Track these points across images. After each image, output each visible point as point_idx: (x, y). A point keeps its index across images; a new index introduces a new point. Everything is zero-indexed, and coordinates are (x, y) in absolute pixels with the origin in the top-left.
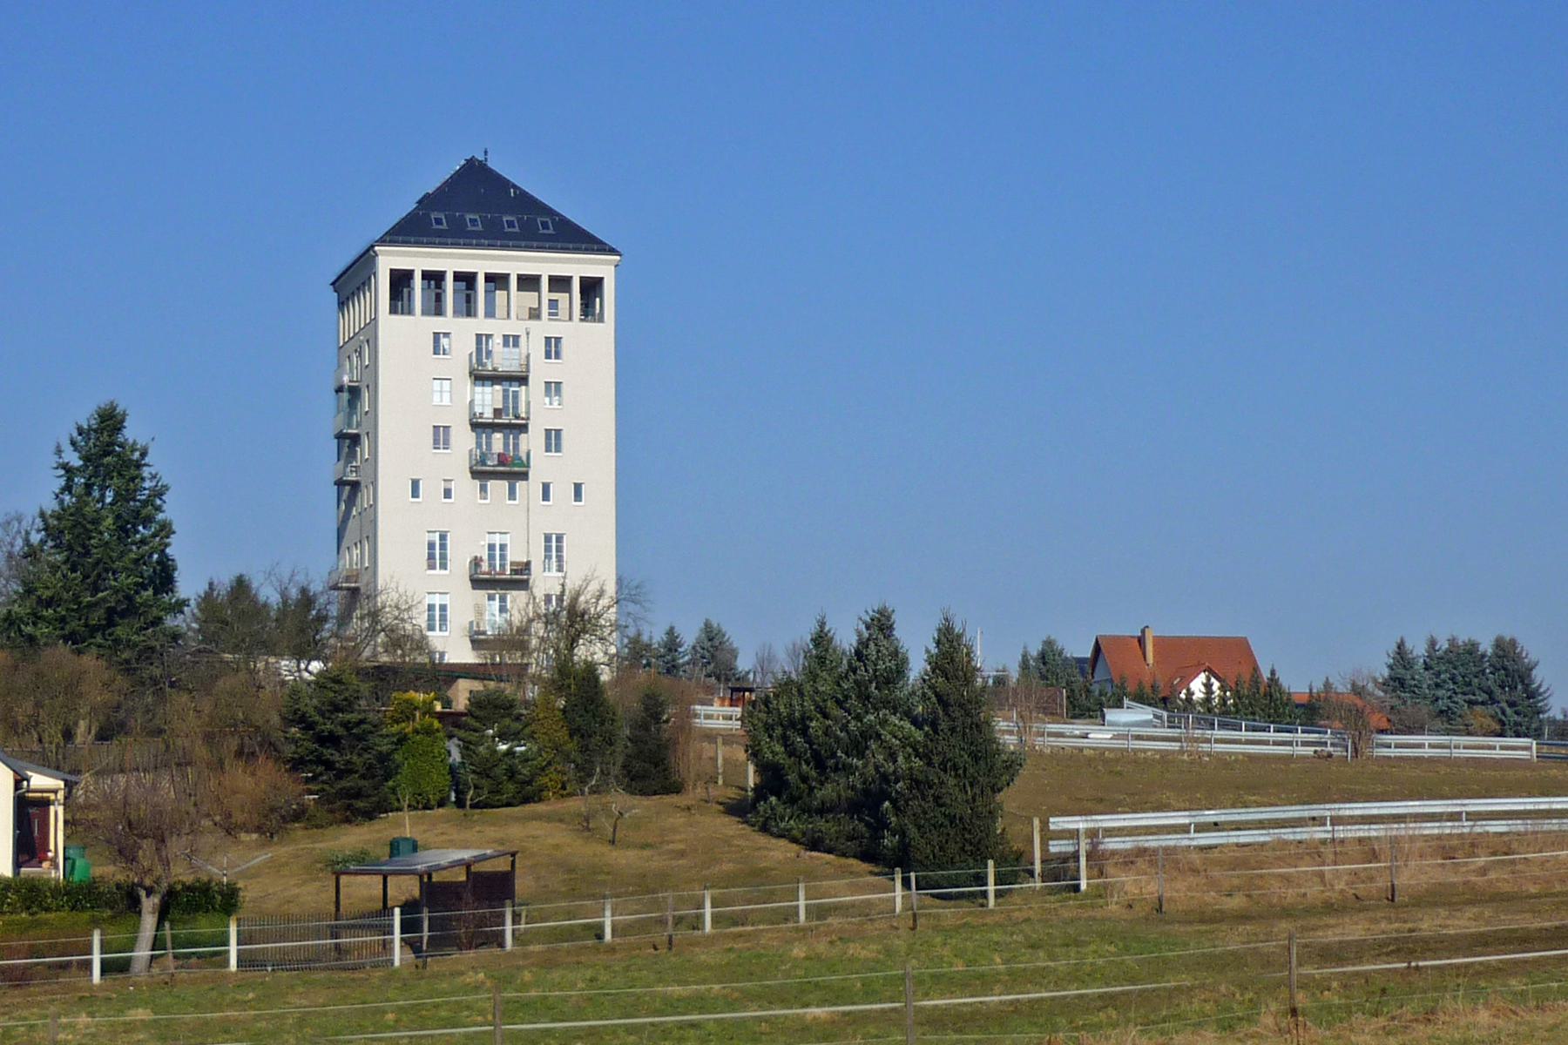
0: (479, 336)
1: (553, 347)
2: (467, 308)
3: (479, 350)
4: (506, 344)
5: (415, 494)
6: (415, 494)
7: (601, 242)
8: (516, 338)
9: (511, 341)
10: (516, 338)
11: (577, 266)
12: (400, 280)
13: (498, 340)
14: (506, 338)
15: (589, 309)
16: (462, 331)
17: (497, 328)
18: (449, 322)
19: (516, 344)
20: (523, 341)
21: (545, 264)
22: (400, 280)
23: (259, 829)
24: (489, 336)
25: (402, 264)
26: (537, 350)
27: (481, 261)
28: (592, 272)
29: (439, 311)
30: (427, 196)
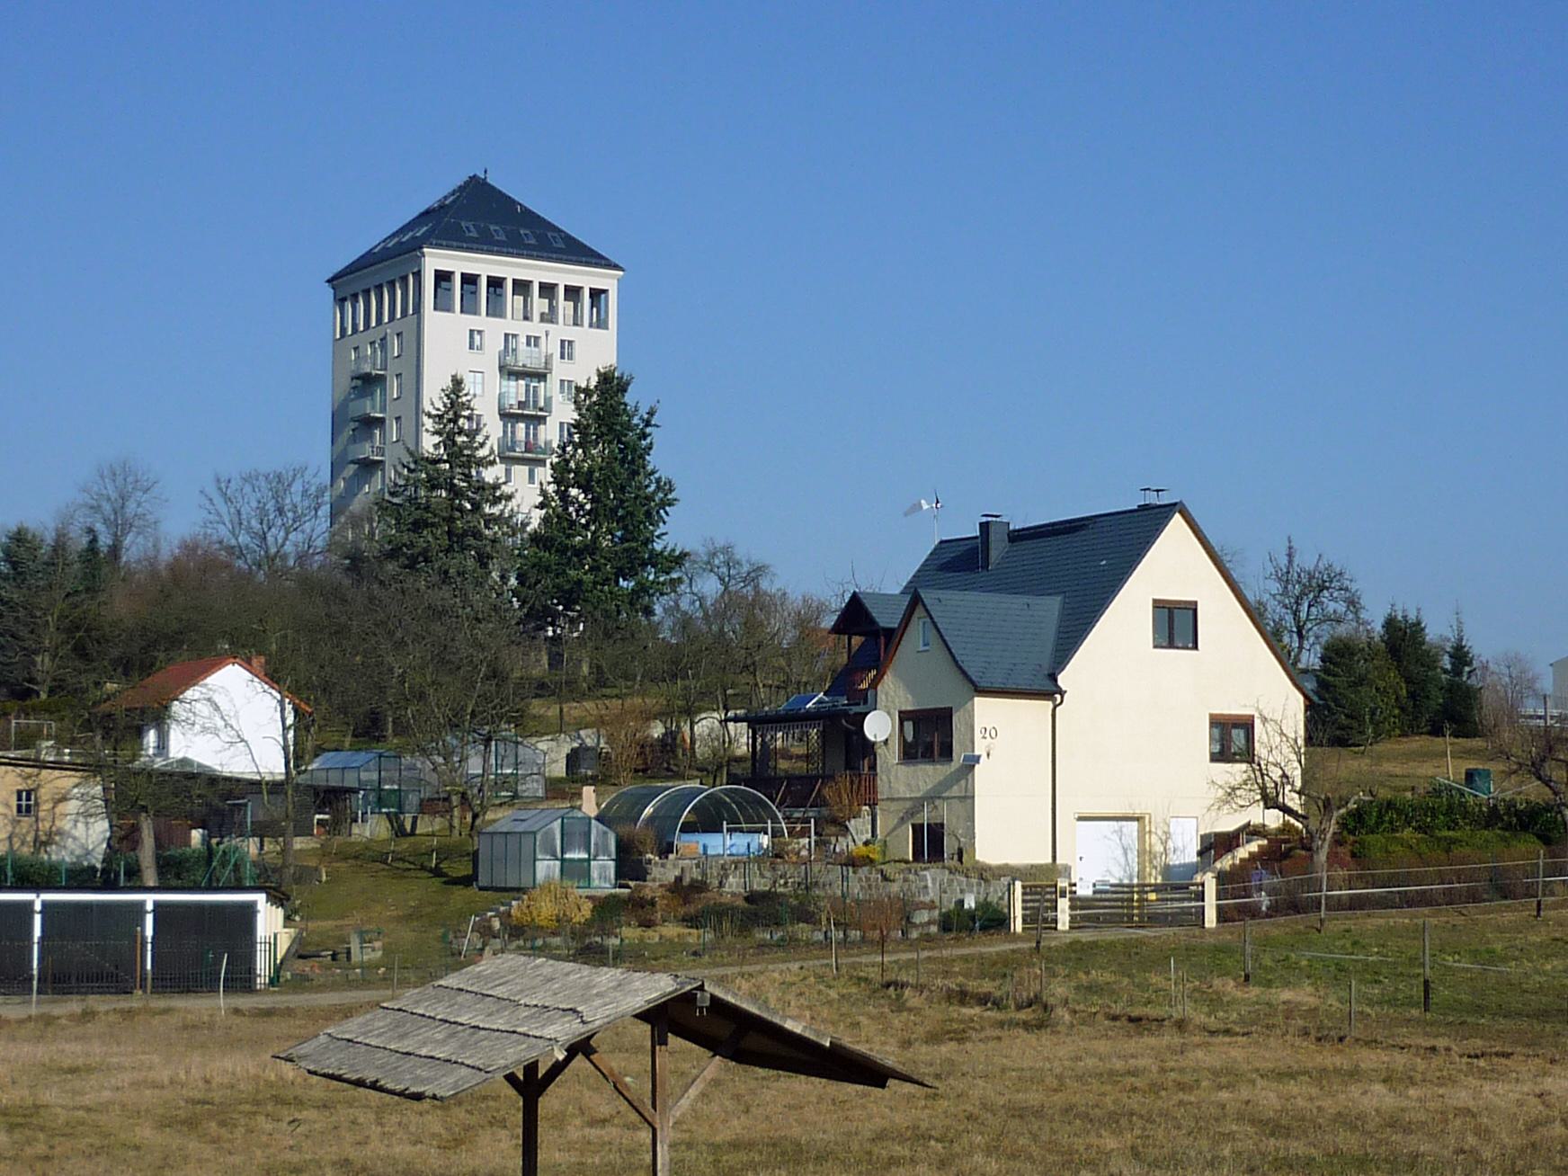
2: (496, 310)
4: (528, 344)
8: (537, 338)
9: (533, 341)
10: (537, 338)
14: (528, 338)
16: (494, 330)
18: (481, 321)
27: (485, 265)
29: (476, 312)
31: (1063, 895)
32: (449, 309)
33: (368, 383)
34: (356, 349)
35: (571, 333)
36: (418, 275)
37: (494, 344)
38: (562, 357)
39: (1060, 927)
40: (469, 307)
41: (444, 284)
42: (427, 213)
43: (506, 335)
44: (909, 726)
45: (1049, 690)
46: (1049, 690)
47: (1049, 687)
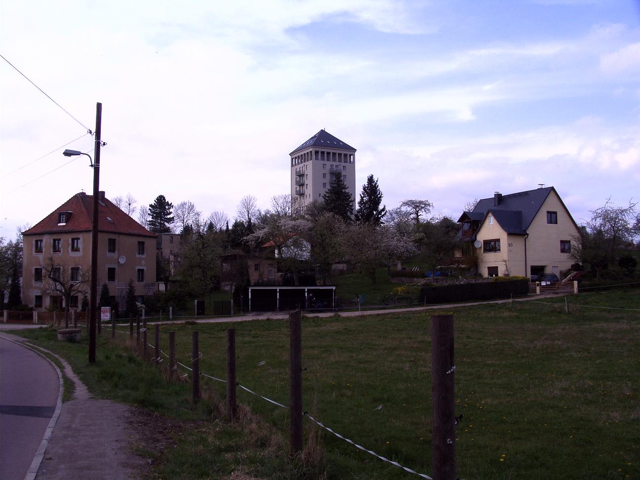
9: (337, 166)
17: (335, 164)
24: (333, 165)
31: (538, 286)
37: (328, 167)
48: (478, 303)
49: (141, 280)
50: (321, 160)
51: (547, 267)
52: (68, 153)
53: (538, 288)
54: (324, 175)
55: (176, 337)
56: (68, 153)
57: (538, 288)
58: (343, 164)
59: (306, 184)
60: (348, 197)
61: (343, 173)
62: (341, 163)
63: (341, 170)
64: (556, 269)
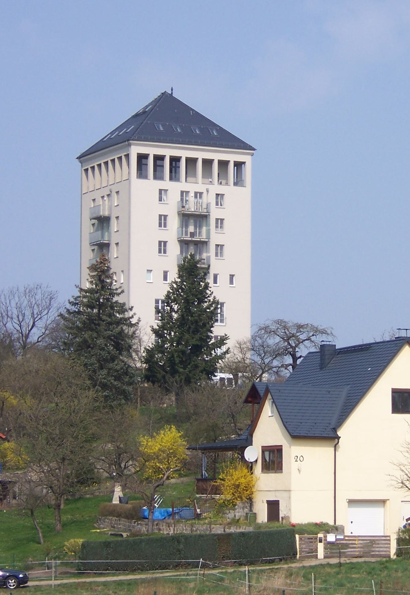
0: (182, 192)
1: (219, 196)
2: (174, 175)
3: (182, 199)
4: (196, 197)
5: (231, 282)
6: (231, 282)
7: (244, 142)
8: (201, 194)
9: (198, 195)
10: (201, 194)
11: (232, 157)
12: (142, 158)
13: (192, 194)
14: (196, 193)
15: (239, 182)
16: (174, 189)
17: (192, 187)
18: (166, 184)
19: (201, 197)
20: (204, 195)
21: (217, 155)
22: (142, 158)
23: (182, 321)
24: (187, 192)
25: (143, 150)
26: (212, 199)
27: (184, 152)
28: (240, 158)
29: (161, 178)
30: (328, 524)
31: (321, 541)
32: (146, 177)
33: (103, 222)
34: (94, 200)
35: (221, 189)
36: (127, 156)
37: (173, 198)
38: (217, 204)
39: (319, 557)
40: (158, 176)
41: (159, 162)
42: (137, 115)
43: (160, 191)
44: (267, 454)
45: (330, 437)
46: (330, 437)
47: (332, 435)
48: (268, 567)
49: (388, 538)
50: (155, 178)
51: (388, 501)
52: (232, 276)
53: (321, 547)
54: (163, 220)
55: (91, 540)
56: (232, 276)
57: (321, 547)
58: (216, 188)
59: (212, 271)
60: (175, 286)
61: (215, 213)
62: (210, 187)
63: (208, 205)
64: (378, 511)
